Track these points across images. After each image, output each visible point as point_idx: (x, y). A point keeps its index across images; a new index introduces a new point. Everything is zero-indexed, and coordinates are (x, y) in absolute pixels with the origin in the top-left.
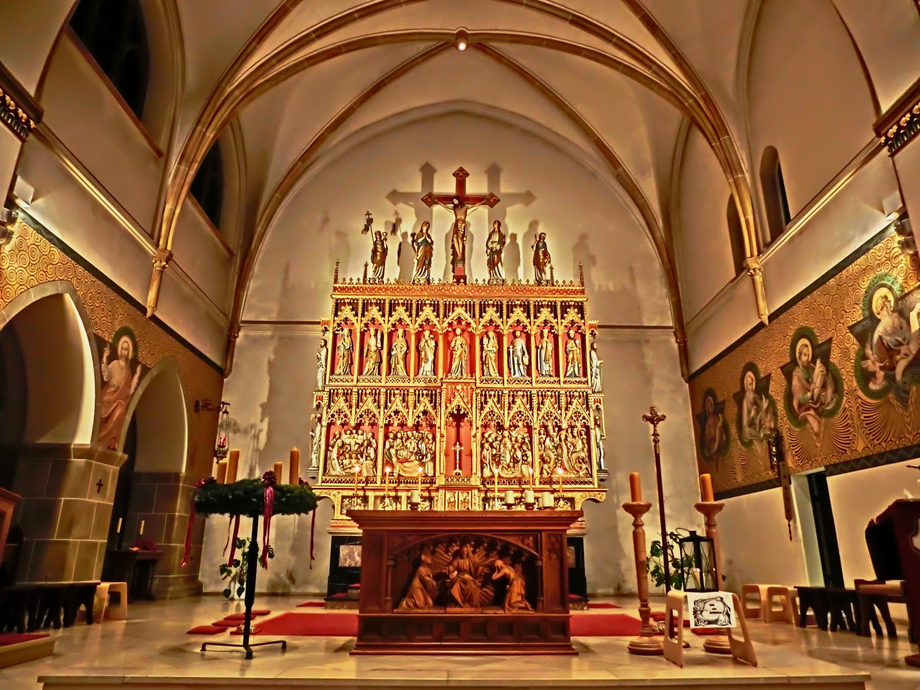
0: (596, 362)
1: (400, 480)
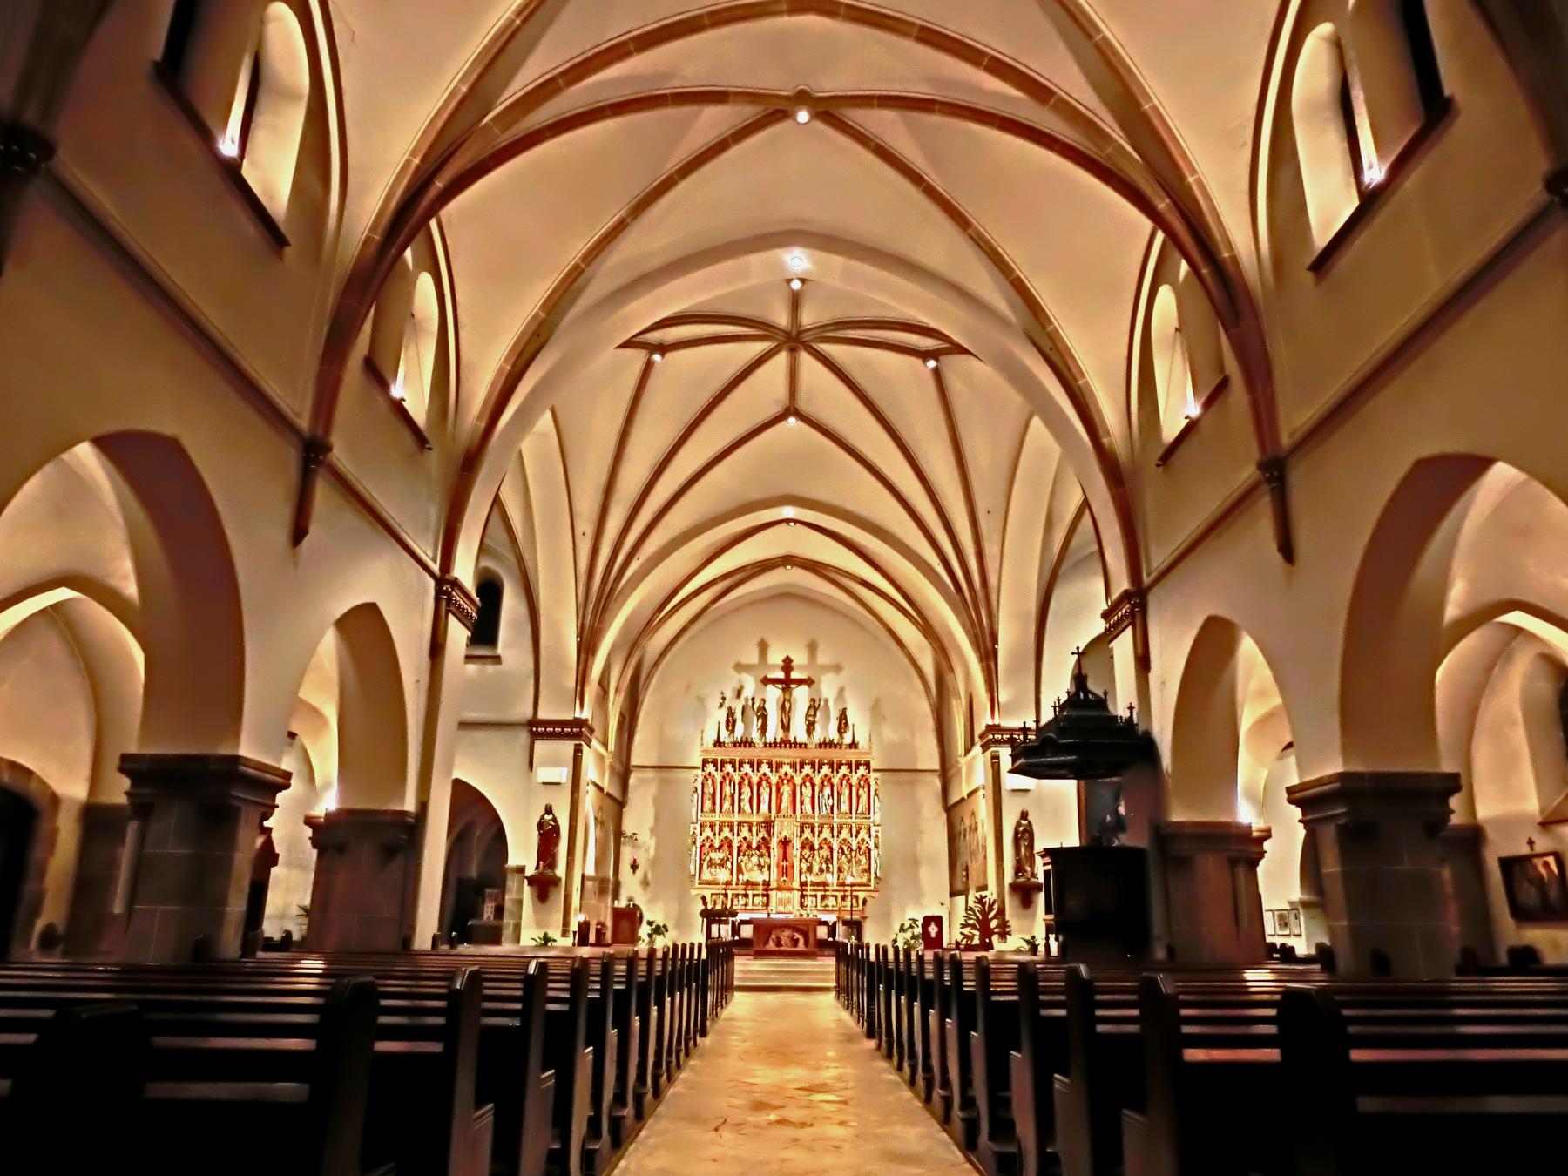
0: (877, 804)
1: (748, 883)
